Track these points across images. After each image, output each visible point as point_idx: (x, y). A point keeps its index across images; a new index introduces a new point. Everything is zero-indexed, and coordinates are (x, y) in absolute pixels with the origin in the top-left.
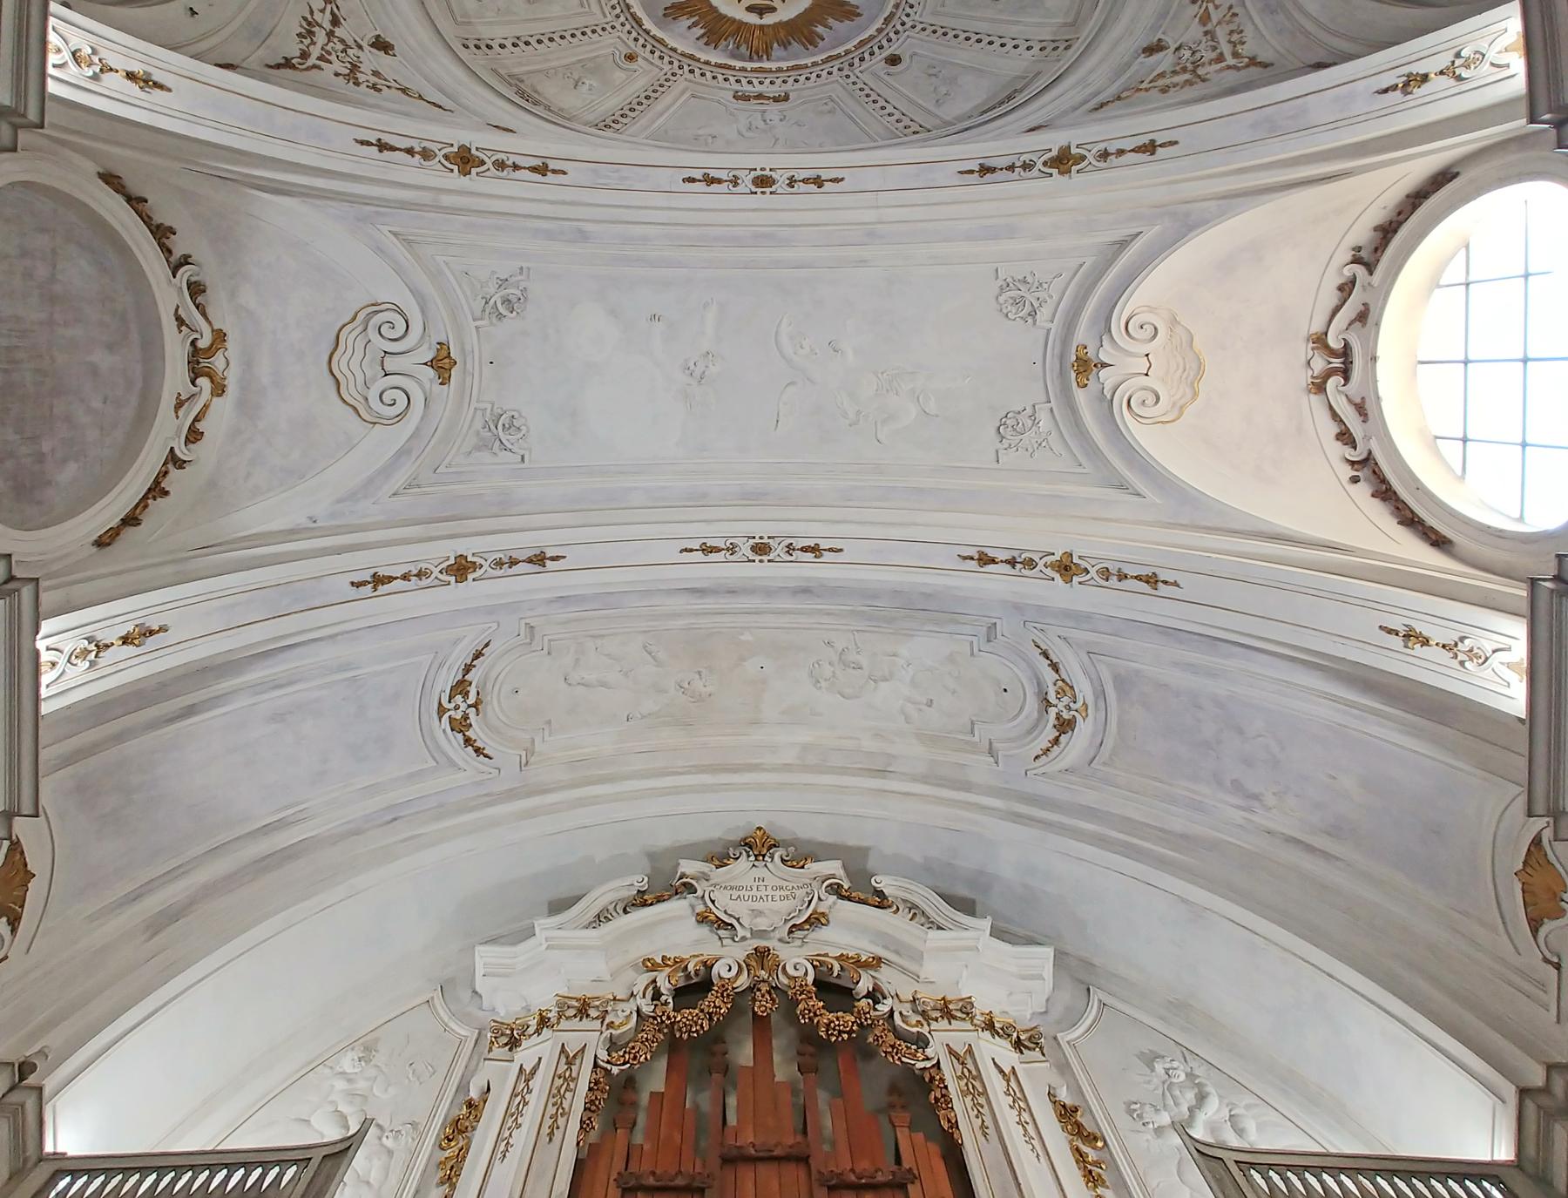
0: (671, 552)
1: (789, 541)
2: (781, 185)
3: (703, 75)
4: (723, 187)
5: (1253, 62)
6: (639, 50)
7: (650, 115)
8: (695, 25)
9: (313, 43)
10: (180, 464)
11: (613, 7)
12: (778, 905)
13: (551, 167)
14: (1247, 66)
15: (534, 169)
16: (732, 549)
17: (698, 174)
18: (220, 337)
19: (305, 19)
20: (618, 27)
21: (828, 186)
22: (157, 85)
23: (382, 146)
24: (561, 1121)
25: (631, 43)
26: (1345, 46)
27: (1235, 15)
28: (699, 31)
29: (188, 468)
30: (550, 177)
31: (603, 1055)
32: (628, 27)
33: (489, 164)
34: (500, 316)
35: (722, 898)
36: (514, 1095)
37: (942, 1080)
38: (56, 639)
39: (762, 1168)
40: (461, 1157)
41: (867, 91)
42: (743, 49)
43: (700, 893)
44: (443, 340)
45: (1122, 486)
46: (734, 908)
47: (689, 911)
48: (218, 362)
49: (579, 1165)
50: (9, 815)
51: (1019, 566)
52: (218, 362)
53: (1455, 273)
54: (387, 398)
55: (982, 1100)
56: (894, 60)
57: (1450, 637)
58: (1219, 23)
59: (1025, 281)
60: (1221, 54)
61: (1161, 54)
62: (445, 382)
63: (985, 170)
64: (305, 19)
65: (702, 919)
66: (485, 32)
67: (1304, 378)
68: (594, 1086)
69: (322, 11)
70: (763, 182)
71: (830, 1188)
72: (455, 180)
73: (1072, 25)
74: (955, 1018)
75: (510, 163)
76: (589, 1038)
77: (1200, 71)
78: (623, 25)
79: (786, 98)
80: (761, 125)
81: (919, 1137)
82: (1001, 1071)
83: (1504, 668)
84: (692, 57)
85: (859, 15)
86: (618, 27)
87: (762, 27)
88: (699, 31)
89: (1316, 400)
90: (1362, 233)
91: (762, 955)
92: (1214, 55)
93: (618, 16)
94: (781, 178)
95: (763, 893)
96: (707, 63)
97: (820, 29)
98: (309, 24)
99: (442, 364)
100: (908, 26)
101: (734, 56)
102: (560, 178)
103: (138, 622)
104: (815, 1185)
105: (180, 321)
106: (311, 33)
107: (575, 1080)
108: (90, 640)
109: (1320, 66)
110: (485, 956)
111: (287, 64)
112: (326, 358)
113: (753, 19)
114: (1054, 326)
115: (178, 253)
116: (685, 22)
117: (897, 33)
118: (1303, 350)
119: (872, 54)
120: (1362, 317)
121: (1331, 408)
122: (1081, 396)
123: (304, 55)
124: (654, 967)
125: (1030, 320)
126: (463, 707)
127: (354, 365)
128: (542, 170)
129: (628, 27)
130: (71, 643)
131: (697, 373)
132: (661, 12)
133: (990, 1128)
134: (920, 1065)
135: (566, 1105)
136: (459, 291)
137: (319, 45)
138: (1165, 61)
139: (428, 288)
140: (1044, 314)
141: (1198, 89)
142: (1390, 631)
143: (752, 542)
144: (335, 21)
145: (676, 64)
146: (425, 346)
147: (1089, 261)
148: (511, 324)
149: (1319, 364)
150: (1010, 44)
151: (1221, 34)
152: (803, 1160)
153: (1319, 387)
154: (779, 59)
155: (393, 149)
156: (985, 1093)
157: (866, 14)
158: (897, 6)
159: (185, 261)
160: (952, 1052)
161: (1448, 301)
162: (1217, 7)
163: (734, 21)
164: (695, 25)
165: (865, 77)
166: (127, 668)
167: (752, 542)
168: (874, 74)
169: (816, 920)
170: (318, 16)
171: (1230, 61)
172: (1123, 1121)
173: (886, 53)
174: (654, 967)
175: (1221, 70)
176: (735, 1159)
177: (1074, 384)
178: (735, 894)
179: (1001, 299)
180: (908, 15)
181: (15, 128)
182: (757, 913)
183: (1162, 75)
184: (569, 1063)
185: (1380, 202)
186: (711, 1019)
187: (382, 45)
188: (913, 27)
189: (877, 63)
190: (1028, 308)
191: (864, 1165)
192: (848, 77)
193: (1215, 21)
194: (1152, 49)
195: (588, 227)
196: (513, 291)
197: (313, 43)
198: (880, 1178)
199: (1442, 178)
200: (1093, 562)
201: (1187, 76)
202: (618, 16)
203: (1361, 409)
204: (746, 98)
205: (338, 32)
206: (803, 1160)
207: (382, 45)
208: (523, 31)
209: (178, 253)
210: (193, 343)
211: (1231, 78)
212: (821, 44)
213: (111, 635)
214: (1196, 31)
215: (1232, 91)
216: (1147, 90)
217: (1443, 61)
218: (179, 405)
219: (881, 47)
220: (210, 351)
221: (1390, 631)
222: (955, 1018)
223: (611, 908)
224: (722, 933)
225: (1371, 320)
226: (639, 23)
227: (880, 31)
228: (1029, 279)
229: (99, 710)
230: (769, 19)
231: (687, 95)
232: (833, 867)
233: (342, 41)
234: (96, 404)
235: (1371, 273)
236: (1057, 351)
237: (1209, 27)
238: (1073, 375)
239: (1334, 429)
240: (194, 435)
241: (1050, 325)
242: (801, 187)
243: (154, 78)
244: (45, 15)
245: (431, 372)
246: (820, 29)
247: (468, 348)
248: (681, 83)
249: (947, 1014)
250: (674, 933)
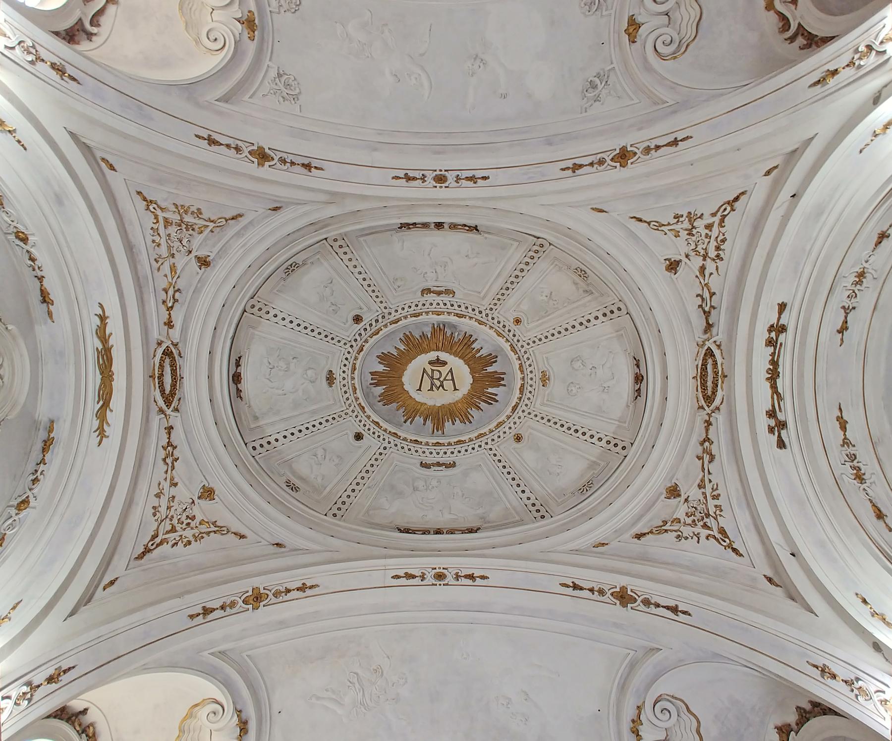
2: (450, 579)
7: (506, 274)
20: (525, 345)
25: (517, 333)
27: (157, 261)
30: (570, 164)
32: (519, 345)
34: (598, 76)
41: (373, 295)
44: (634, 46)
57: (40, 65)
63: (308, 167)
69: (711, 274)
75: (595, 166)
79: (423, 292)
80: (439, 269)
83: (9, 34)
86: (525, 345)
87: (438, 350)
88: (476, 346)
93: (525, 352)
96: (405, 439)
97: (402, 347)
98: (718, 256)
100: (348, 345)
102: (564, 165)
112: (704, 11)
113: (444, 356)
114: (267, 62)
119: (371, 325)
122: (253, 8)
125: (281, 72)
128: (576, 167)
129: (519, 345)
131: (478, 61)
136: (625, 86)
140: (273, 73)
142: (74, 79)
144: (703, 269)
146: (643, 37)
147: (246, 98)
148: (590, 74)
154: (425, 324)
168: (369, 309)
177: (256, 15)
179: (298, 91)
180: (349, 353)
189: (367, 318)
190: (283, 79)
192: (386, 308)
196: (591, 94)
202: (525, 352)
208: (584, 334)
212: (401, 336)
217: (846, 59)
219: (365, 329)
221: (74, 79)
228: (281, 99)
230: (433, 355)
235: (80, 19)
236: (265, 45)
238: (256, 21)
241: (270, 64)
242: (418, 174)
246: (402, 347)
247: (617, 49)
248: (485, 305)
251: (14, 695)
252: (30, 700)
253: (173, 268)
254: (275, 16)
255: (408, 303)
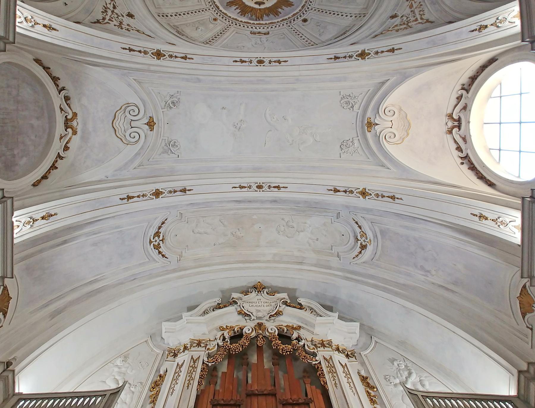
0: (229, 188)
1: (269, 184)
2: (267, 63)
3: (240, 25)
4: (247, 64)
5: (428, 21)
6: (218, 17)
7: (222, 39)
8: (237, 8)
9: (107, 15)
10: (61, 158)
11: (209, 3)
12: (266, 308)
13: (188, 57)
14: (426, 22)
15: (182, 58)
16: (250, 187)
17: (238, 59)
18: (75, 115)
19: (104, 6)
20: (211, 9)
21: (282, 63)
22: (53, 29)
23: (131, 50)
24: (191, 382)
25: (215, 15)
26: (459, 16)
27: (421, 5)
28: (238, 11)
29: (64, 159)
30: (188, 60)
31: (206, 359)
32: (214, 9)
33: (167, 56)
34: (171, 108)
35: (246, 306)
36: (175, 373)
37: (321, 368)
38: (19, 218)
39: (260, 398)
40: (157, 394)
41: (296, 31)
42: (254, 17)
43: (239, 304)
44: (151, 116)
45: (383, 166)
46: (250, 309)
47: (235, 310)
48: (74, 123)
49: (198, 397)
50: (3, 278)
51: (348, 193)
52: (74, 123)
53: (496, 93)
54: (132, 135)
55: (335, 375)
56: (305, 21)
58: (416, 8)
59: (350, 96)
60: (417, 18)
61: (396, 19)
62: (152, 130)
63: (336, 58)
64: (104, 6)
65: (240, 313)
66: (166, 11)
67: (445, 129)
68: (203, 370)
69: (110, 4)
70: (260, 62)
71: (283, 405)
72: (155, 61)
73: (366, 8)
74: (326, 347)
75: (174, 55)
76: (201, 354)
77: (410, 24)
78: (213, 8)
79: (268, 33)
80: (260, 42)
81: (314, 387)
82: (342, 365)
84: (236, 19)
85: (293, 5)
86: (211, 9)
87: (260, 9)
88: (238, 11)
89: (449, 136)
90: (465, 79)
91: (260, 325)
92: (414, 19)
93: (211, 6)
94: (267, 61)
95: (260, 304)
96: (241, 21)
97: (280, 10)
98: (106, 8)
99: (151, 124)
100: (310, 9)
101: (250, 19)
102: (191, 61)
103: (47, 212)
104: (278, 404)
105: (62, 109)
106: (106, 11)
107: (196, 368)
108: (31, 218)
109: (450, 22)
110: (166, 326)
111: (98, 22)
112: (111, 122)
113: (257, 6)
114: (359, 111)
115: (61, 86)
116: (234, 8)
117: (306, 11)
118: (445, 119)
119: (298, 18)
120: (465, 108)
121: (454, 139)
122: (369, 135)
123: (104, 19)
124: (223, 329)
125: (351, 109)
126: (158, 241)
127: (121, 124)
128: (185, 58)
129: (214, 9)
130: (24, 219)
131: (238, 127)
132: (225, 4)
133: (338, 384)
134: (314, 363)
135: (193, 376)
136: (156, 99)
137: (109, 15)
138: (397, 21)
139: (146, 98)
140: (356, 107)
141: (409, 30)
143: (256, 184)
144: (114, 7)
145: (231, 22)
146: (145, 118)
147: (372, 89)
148: (174, 110)
149: (450, 124)
150: (345, 15)
151: (417, 11)
152: (274, 395)
153: (450, 132)
154: (266, 20)
155: (134, 51)
156: (336, 372)
157: (295, 5)
158: (306, 2)
159: (63, 89)
160: (325, 358)
161: (494, 102)
162: (415, 2)
163: (250, 7)
164: (237, 8)
165: (295, 26)
166: (43, 228)
167: (256, 184)
168: (298, 25)
169: (279, 313)
170: (108, 6)
171: (420, 21)
172: (383, 382)
173: (302, 18)
174: (223, 329)
175: (417, 24)
176: (251, 395)
177: (367, 131)
178: (251, 304)
179: (342, 102)
180: (310, 5)
181: (5, 44)
182: (258, 311)
183: (396, 26)
184: (194, 362)
185: (471, 69)
186: (242, 347)
187: (130, 15)
188: (312, 9)
190: (351, 105)
191: (295, 397)
192: (289, 26)
193: (414, 7)
194: (393, 17)
195: (201, 77)
196: (175, 99)
197: (107, 15)
198: (300, 401)
199: (492, 61)
200: (373, 191)
201: (405, 26)
202: (211, 6)
203: (464, 139)
204: (255, 33)
205: (115, 11)
206: (274, 395)
207: (130, 15)
208: (178, 10)
209: (61, 86)
210: (66, 117)
211: (420, 26)
212: (280, 15)
213: (38, 216)
214: (408, 11)
215: (421, 31)
216: (391, 31)
217: (493, 21)
218: (61, 138)
219: (301, 16)
220: (72, 120)
222: (326, 347)
223: (208, 309)
224: (246, 318)
225: (468, 109)
226: (218, 8)
227: (300, 10)
228: (351, 95)
229: (34, 242)
230: (262, 7)
231: (235, 32)
232: (284, 295)
233: (117, 14)
234: (33, 138)
236: (361, 120)
237: (413, 9)
238: (366, 128)
239: (455, 146)
240: (66, 148)
241: (358, 111)
242: (273, 64)
243: (53, 27)
244: (15, 5)
245: (147, 127)
246: (280, 10)
247: (160, 118)
248: (232, 28)
249: (323, 345)
250: (230, 318)
251: (507, 23)
252: (497, 19)
253: (411, 6)
254: (356, 136)
255: (276, 29)
